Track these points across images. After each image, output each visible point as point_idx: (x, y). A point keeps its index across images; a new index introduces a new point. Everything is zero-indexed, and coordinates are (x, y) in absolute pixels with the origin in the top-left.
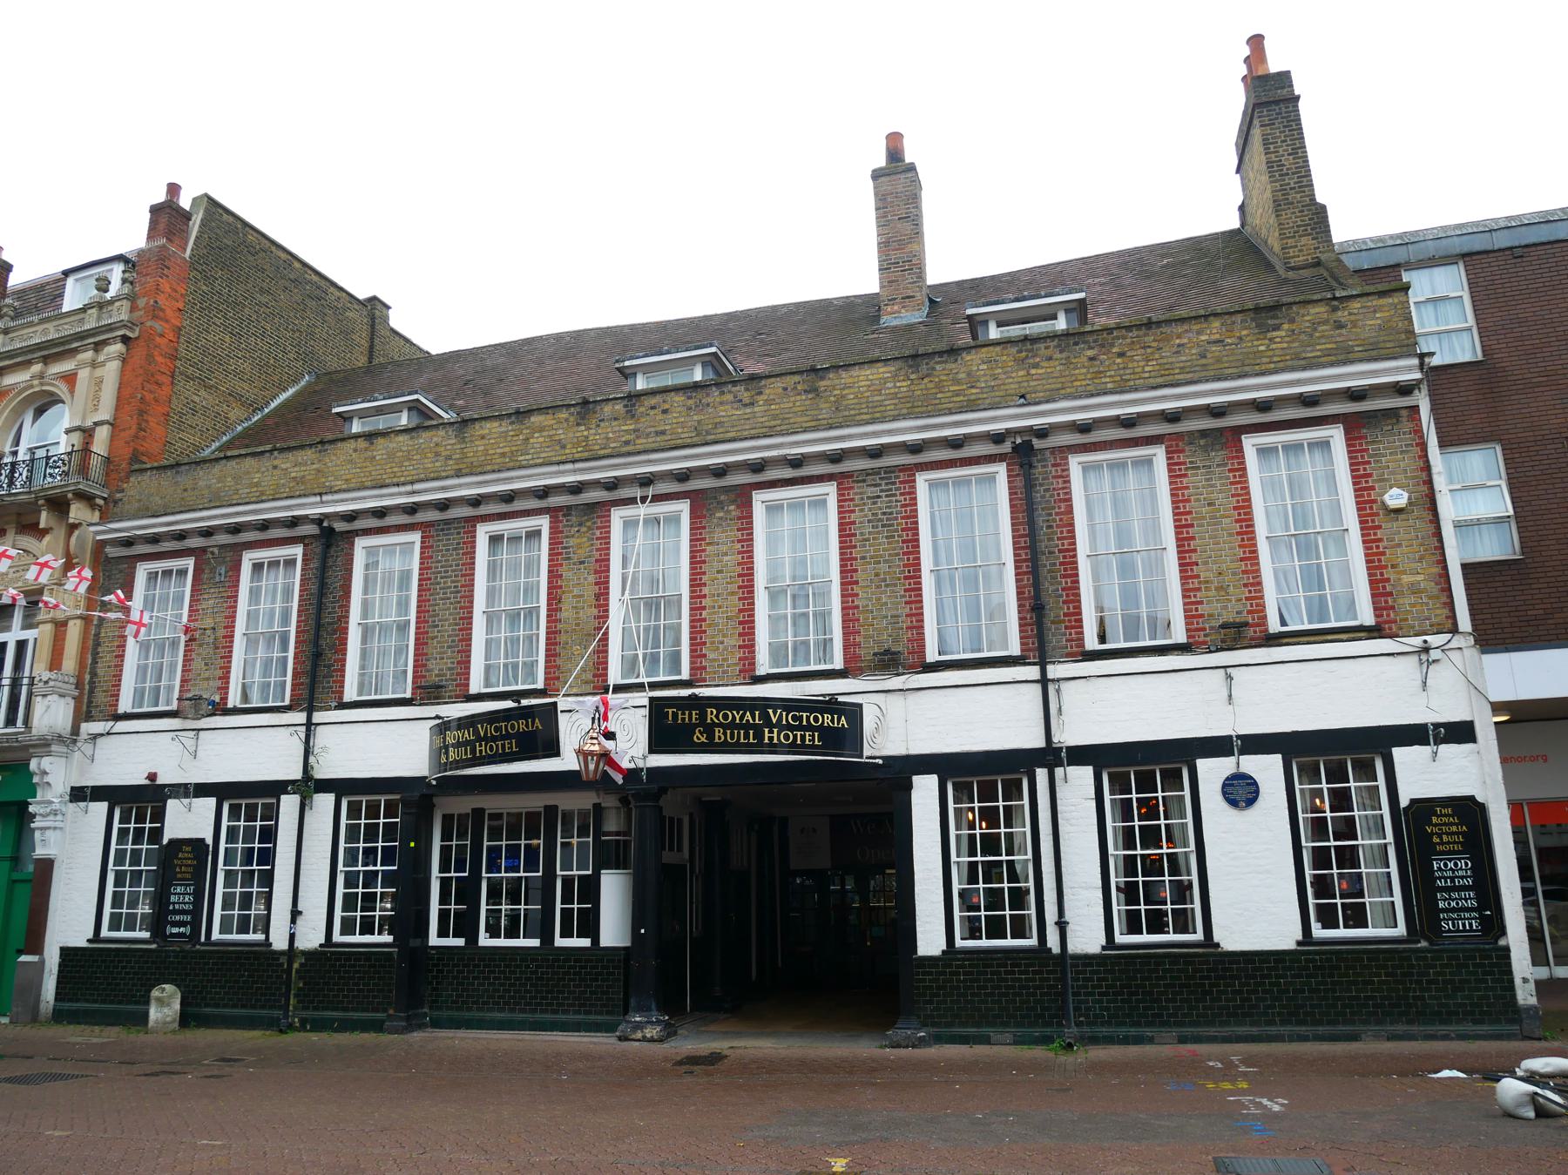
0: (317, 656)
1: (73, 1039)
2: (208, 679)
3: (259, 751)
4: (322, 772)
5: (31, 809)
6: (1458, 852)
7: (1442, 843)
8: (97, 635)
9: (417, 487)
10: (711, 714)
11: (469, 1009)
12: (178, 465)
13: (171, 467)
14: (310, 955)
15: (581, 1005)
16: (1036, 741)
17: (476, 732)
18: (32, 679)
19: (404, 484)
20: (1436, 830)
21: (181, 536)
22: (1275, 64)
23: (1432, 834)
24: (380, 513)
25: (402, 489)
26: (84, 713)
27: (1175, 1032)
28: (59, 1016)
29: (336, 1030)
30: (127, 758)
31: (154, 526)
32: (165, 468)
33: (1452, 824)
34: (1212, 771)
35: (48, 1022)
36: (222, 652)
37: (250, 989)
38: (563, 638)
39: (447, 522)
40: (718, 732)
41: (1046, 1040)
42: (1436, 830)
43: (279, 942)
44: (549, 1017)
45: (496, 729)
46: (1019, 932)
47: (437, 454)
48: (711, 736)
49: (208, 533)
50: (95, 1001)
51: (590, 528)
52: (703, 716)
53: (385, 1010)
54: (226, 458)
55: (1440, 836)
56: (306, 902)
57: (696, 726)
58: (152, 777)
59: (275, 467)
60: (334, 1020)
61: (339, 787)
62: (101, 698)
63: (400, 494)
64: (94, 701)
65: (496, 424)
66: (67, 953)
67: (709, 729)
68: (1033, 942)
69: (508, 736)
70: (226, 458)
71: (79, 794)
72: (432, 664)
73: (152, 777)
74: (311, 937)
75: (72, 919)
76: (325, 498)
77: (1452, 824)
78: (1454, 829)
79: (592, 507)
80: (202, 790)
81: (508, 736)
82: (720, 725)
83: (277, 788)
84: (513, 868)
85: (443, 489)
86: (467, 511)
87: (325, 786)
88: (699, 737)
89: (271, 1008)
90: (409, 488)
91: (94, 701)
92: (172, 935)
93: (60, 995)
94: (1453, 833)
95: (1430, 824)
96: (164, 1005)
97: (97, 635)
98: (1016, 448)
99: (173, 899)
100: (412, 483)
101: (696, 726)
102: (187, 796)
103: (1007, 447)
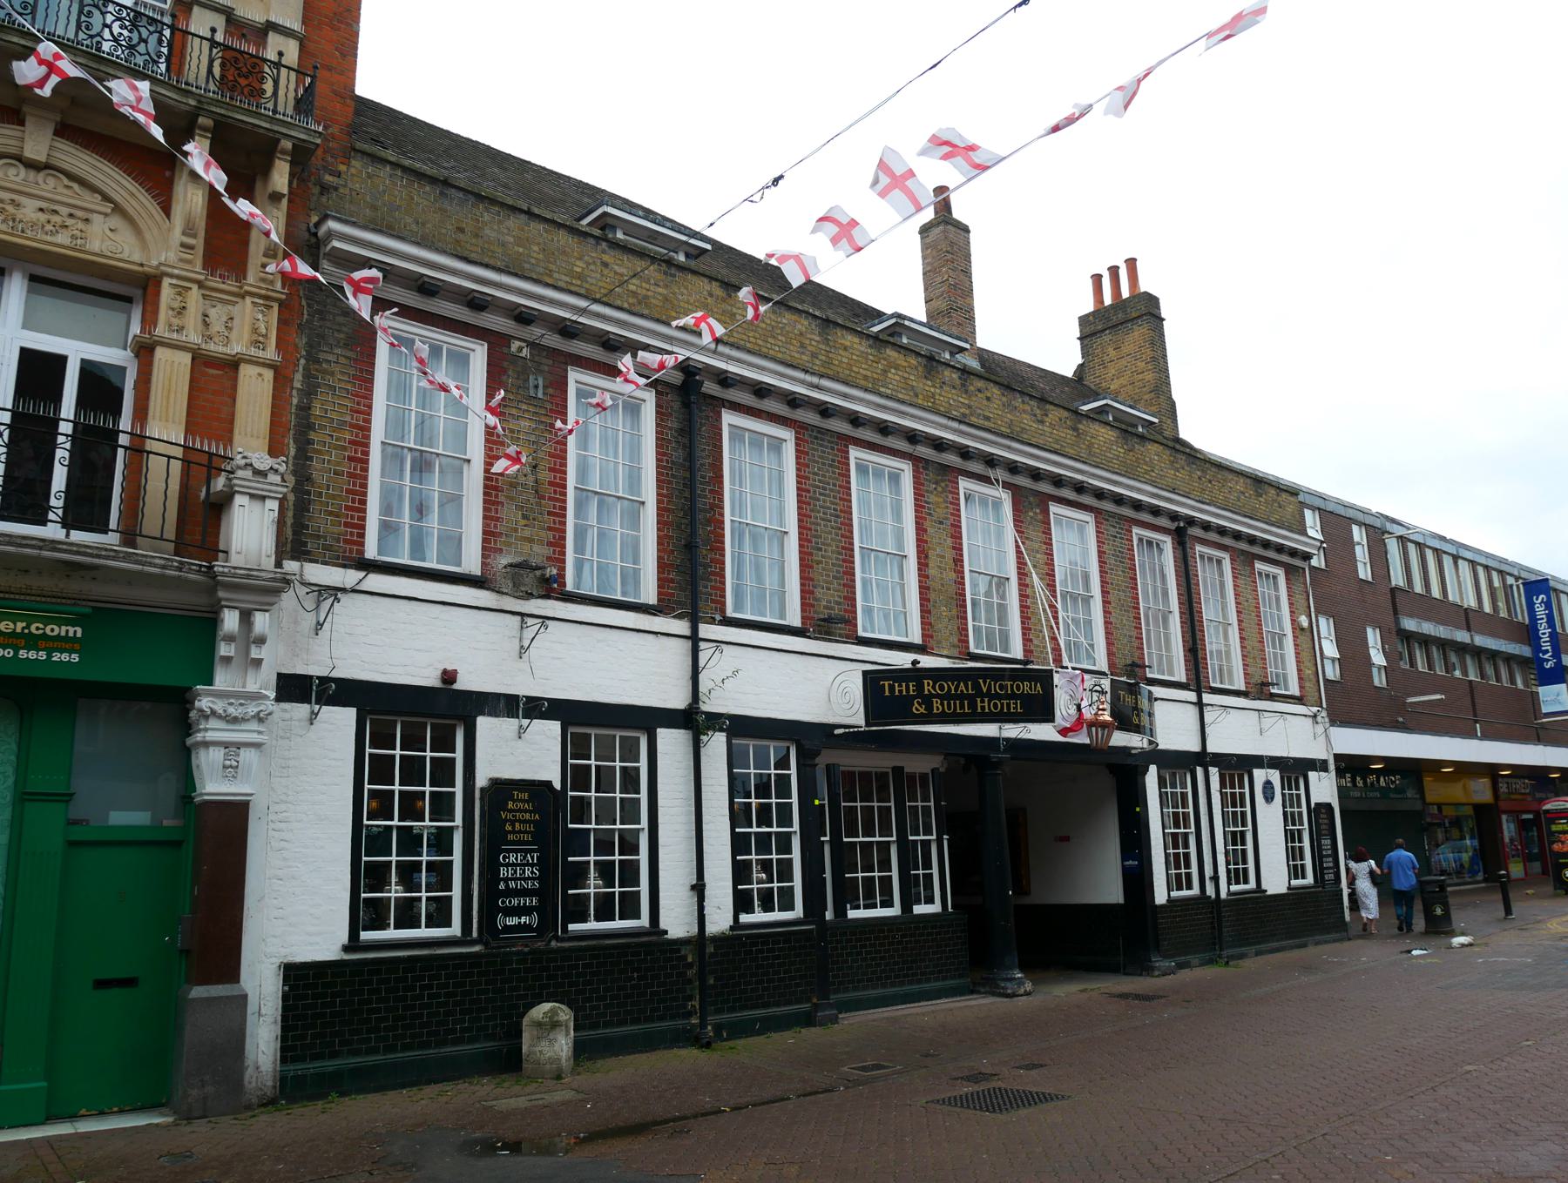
0: (690, 547)
1: (504, 1104)
2: (530, 540)
3: (630, 664)
4: (712, 704)
5: (204, 703)
6: (528, 843)
7: (513, 832)
8: (304, 409)
9: (825, 383)
10: (928, 686)
11: (846, 990)
12: (446, 183)
13: (433, 180)
14: (719, 939)
15: (940, 972)
16: (1195, 747)
17: (976, 686)
18: (139, 438)
19: (813, 374)
20: (510, 816)
21: (477, 303)
22: (1145, 286)
23: (506, 820)
24: (761, 390)
25: (809, 378)
26: (295, 541)
27: (1253, 949)
28: (294, 1087)
29: (759, 1033)
30: (398, 638)
31: (454, 272)
32: (420, 175)
33: (526, 811)
34: (1260, 775)
35: (269, 1103)
36: (548, 505)
37: (650, 989)
38: (932, 596)
39: (821, 431)
40: (936, 703)
41: (1211, 962)
42: (510, 816)
43: (676, 922)
44: (915, 987)
45: (1001, 687)
46: (630, 910)
47: (802, 346)
48: (929, 707)
49: (523, 317)
50: (375, 1051)
51: (944, 491)
52: (920, 687)
53: (809, 1000)
54: (529, 213)
55: (513, 824)
56: (691, 872)
57: (915, 697)
58: (449, 677)
59: (605, 265)
60: (754, 1021)
61: (740, 727)
62: (322, 522)
63: (803, 382)
64: (321, 526)
65: (856, 340)
66: (298, 977)
67: (927, 701)
68: (1196, 891)
69: (1013, 696)
70: (529, 213)
71: (293, 688)
72: (819, 592)
73: (449, 677)
74: (720, 919)
75: (299, 905)
76: (721, 348)
77: (526, 811)
78: (527, 816)
79: (945, 469)
80: (535, 708)
81: (1013, 696)
82: (937, 696)
83: (649, 719)
84: (869, 832)
85: (845, 396)
86: (842, 427)
87: (715, 721)
88: (918, 708)
89: (673, 1017)
90: (815, 380)
91: (321, 526)
92: (508, 929)
93: (290, 1046)
94: (525, 822)
95: (506, 810)
96: (550, 1032)
97: (304, 409)
98: (1178, 528)
99: (503, 872)
100: (821, 376)
101: (915, 697)
102: (512, 713)
103: (1173, 526)
